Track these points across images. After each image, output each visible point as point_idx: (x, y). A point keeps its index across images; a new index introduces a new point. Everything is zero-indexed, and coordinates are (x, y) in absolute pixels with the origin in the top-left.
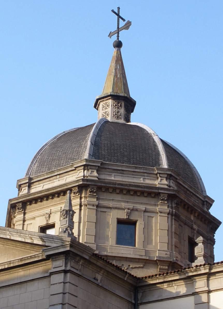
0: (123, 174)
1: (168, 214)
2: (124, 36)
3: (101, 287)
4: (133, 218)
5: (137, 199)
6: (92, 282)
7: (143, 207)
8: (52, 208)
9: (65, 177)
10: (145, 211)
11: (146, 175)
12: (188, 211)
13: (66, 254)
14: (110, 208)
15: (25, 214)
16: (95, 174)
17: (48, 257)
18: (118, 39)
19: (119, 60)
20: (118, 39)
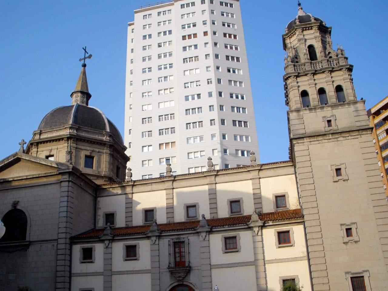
0: (88, 132)
1: (109, 154)
2: (87, 61)
3: (83, 189)
4: (93, 155)
5: (94, 146)
6: (79, 186)
7: (97, 150)
8: (52, 147)
9: (59, 132)
10: (99, 152)
11: (99, 134)
12: (117, 153)
13: (69, 173)
14: (82, 149)
15: (37, 148)
16: (75, 132)
17: (60, 174)
18: (84, 62)
19: (84, 73)
20: (84, 62)
